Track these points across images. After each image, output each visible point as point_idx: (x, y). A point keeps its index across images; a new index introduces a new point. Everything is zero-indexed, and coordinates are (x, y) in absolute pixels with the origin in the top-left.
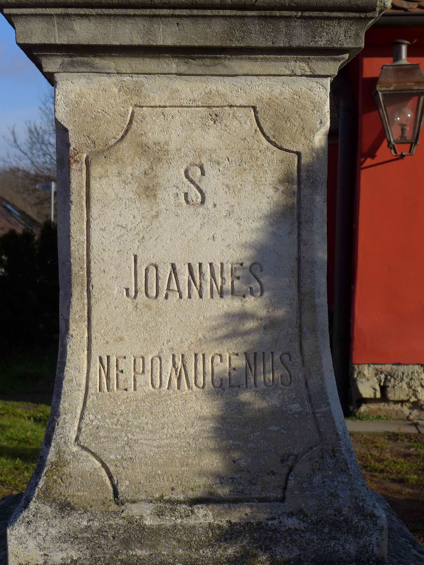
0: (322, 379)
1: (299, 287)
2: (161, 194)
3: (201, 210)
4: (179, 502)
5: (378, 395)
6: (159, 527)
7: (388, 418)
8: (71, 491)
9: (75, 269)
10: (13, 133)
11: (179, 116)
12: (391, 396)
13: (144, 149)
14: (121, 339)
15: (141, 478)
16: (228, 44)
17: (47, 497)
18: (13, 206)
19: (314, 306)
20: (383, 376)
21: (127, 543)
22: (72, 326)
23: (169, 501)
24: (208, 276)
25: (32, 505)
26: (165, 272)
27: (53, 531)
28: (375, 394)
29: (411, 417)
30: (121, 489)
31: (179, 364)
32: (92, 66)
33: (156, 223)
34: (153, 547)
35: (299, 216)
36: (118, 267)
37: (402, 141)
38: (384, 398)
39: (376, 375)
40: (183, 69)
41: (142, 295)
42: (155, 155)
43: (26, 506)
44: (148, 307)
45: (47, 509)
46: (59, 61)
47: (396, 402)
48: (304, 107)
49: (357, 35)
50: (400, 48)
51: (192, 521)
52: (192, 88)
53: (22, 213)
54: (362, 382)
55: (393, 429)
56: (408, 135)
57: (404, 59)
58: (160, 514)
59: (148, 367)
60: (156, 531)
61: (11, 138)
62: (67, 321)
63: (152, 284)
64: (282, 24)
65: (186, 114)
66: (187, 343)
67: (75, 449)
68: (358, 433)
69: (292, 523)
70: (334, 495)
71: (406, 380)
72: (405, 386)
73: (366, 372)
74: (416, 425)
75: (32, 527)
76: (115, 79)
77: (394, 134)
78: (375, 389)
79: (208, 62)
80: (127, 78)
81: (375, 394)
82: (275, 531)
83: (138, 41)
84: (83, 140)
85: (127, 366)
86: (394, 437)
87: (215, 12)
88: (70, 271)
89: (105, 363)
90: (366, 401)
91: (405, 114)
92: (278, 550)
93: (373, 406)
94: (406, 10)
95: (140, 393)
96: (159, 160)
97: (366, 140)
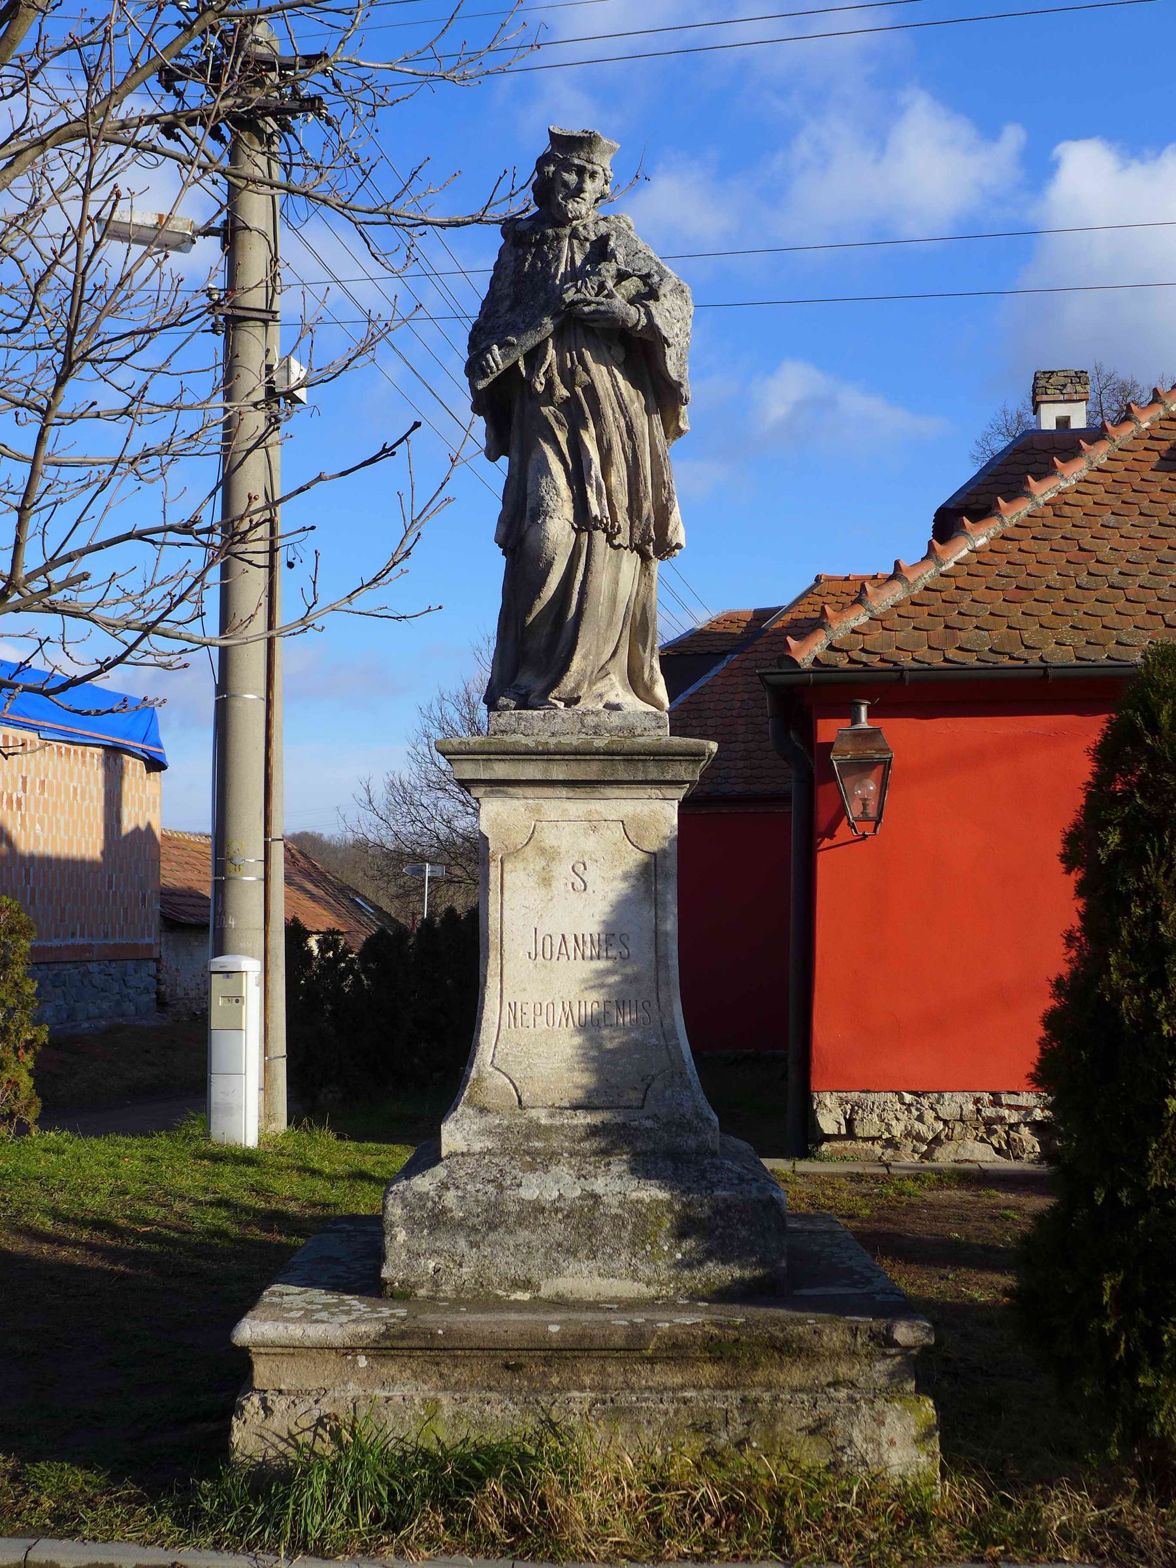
0: (673, 1020)
1: (656, 952)
2: (554, 884)
3: (584, 895)
4: (567, 1108)
5: (844, 1131)
6: (551, 1126)
7: (855, 1158)
8: (487, 1099)
9: (492, 938)
10: (368, 791)
11: (568, 828)
12: (859, 1131)
13: (542, 851)
14: (525, 990)
15: (538, 1091)
16: (602, 778)
17: (470, 1102)
18: (364, 898)
19: (667, 967)
20: (849, 1107)
21: (527, 1137)
22: (489, 980)
23: (559, 1108)
24: (589, 944)
25: (459, 1109)
26: (557, 940)
27: (475, 1127)
28: (839, 1129)
29: (884, 1158)
30: (524, 1098)
31: (567, 1009)
32: (506, 793)
33: (551, 905)
34: (546, 1140)
35: (656, 899)
36: (522, 937)
37: (864, 818)
38: (851, 1135)
39: (841, 1105)
40: (571, 795)
41: (540, 957)
42: (549, 855)
43: (455, 1110)
44: (545, 966)
45: (470, 1111)
46: (483, 789)
47: (866, 1139)
48: (658, 821)
49: (694, 771)
50: (859, 709)
51: (575, 1122)
52: (578, 807)
53: (378, 909)
54: (823, 1114)
55: (857, 1169)
56: (872, 812)
57: (864, 723)
58: (552, 1116)
59: (544, 1011)
60: (549, 1129)
61: (365, 797)
62: (485, 977)
63: (545, 950)
64: (640, 765)
65: (573, 826)
66: (573, 994)
67: (491, 1069)
68: (814, 1174)
69: (648, 1123)
70: (681, 1105)
71: (877, 1111)
72: (876, 1119)
73: (828, 1102)
74: (887, 1166)
75: (459, 1123)
76: (523, 802)
77: (854, 810)
78: (838, 1123)
79: (588, 790)
80: (530, 801)
81: (839, 1129)
82: (636, 1129)
83: (539, 777)
84: (499, 845)
85: (529, 1009)
86: (857, 1178)
87: (593, 757)
88: (488, 939)
89: (513, 1007)
90: (829, 1138)
91: (866, 786)
92: (638, 1144)
93: (837, 1145)
94: (865, 664)
95: (538, 1030)
96: (554, 859)
97: (823, 817)
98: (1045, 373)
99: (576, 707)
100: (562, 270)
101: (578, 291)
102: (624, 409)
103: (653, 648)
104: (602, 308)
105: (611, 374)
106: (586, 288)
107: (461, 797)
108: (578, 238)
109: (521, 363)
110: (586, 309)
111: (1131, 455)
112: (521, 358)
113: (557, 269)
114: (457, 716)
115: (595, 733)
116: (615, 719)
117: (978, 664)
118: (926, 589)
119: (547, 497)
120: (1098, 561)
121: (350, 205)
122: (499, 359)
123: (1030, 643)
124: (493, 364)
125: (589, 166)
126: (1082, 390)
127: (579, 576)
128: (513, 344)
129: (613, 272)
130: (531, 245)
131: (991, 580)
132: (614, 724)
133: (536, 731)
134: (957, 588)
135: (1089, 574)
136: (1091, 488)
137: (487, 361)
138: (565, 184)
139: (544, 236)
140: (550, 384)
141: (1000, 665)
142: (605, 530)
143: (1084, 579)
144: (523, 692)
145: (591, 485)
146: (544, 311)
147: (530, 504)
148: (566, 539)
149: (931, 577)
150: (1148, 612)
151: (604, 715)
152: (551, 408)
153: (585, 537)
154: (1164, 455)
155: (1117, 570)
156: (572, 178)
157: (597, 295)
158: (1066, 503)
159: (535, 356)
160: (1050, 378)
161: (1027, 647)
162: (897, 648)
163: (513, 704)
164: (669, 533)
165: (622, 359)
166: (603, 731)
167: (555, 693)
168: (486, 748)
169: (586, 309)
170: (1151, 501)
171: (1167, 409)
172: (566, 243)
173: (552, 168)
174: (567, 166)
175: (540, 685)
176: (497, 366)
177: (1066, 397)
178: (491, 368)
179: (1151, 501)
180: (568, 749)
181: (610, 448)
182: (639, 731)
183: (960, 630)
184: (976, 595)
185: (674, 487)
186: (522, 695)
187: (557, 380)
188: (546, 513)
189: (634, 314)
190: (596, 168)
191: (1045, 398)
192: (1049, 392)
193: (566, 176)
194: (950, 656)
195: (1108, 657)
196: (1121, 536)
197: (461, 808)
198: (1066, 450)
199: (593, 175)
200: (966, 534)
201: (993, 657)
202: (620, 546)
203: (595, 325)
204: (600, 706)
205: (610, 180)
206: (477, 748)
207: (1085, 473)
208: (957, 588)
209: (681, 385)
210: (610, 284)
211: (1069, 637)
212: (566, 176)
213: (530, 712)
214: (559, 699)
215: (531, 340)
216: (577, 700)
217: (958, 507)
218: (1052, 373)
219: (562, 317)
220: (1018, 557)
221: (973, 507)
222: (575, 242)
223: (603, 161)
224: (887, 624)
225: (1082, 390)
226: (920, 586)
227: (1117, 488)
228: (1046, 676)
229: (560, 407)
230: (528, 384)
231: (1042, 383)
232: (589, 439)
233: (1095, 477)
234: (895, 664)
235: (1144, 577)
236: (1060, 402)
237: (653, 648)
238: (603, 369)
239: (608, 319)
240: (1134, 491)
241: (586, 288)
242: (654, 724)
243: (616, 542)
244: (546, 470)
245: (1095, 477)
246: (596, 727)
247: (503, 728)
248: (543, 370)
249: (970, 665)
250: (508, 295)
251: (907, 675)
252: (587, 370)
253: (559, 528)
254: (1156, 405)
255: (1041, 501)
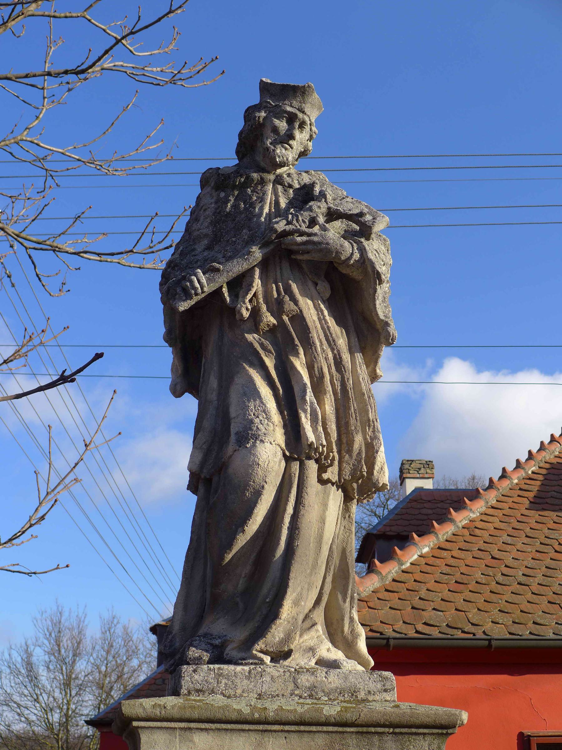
64: (376, 738)
98: (408, 461)
99: (286, 663)
100: (266, 210)
101: (289, 223)
102: (331, 342)
103: (352, 598)
104: (315, 239)
105: (317, 308)
106: (298, 221)
107: (18, 711)
108: (282, 184)
109: (225, 290)
110: (299, 239)
111: (511, 499)
112: (225, 285)
113: (262, 209)
114: (19, 659)
115: (311, 696)
116: (333, 680)
117: (440, 636)
118: (394, 580)
119: (257, 421)
120: (506, 566)
121: (23, 235)
122: (204, 280)
123: (474, 621)
124: (197, 285)
125: (300, 115)
126: (430, 472)
127: (290, 510)
128: (218, 270)
129: (324, 209)
130: (234, 187)
131: (438, 576)
132: (333, 686)
133: (239, 691)
134: (415, 581)
135: (502, 574)
136: (490, 519)
137: (191, 282)
138: (275, 130)
139: (249, 180)
140: (255, 313)
141: (455, 637)
142: (317, 461)
143: (500, 578)
144: (217, 642)
145: (305, 411)
146: (251, 241)
147: (234, 428)
148: (276, 467)
149: (396, 572)
150: (549, 602)
151: (321, 672)
152: (256, 336)
153: (296, 466)
154: (532, 500)
155: (521, 573)
156: (282, 125)
157: (309, 227)
158: (476, 528)
159: (239, 284)
160: (411, 464)
161: (473, 624)
162: (381, 622)
163: (206, 656)
164: (375, 472)
165: (328, 294)
166: (320, 694)
167: (261, 645)
168: (188, 714)
169: (299, 239)
170: (531, 528)
171: (526, 473)
172: (270, 187)
173: (263, 114)
174: (279, 113)
175: (239, 635)
176: (202, 288)
177: (421, 475)
178: (195, 289)
179: (531, 528)
180: (291, 717)
181: (322, 376)
182: (362, 695)
183: (423, 610)
184: (429, 586)
185: (378, 425)
186: (215, 647)
187: (264, 307)
188: (256, 437)
189: (348, 248)
190: (307, 119)
191: (408, 475)
192: (411, 472)
193: (277, 122)
194: (396, 628)
195: (530, 633)
196: (518, 550)
197: (17, 717)
198: (442, 501)
199: (302, 125)
200: (415, 544)
201: (450, 631)
202: (328, 481)
203: (306, 257)
204: (313, 663)
205: (314, 136)
206: (176, 713)
207: (484, 509)
208: (415, 581)
209: (387, 324)
210: (321, 220)
211: (500, 618)
212: (277, 122)
213: (232, 667)
214: (265, 653)
215: (237, 267)
216: (287, 654)
217: (378, 533)
218: (413, 461)
219: (272, 247)
220: (452, 562)
221: (388, 533)
222: (280, 188)
223: (312, 113)
224: (370, 604)
225: (430, 472)
226: (390, 578)
227: (506, 519)
228: (490, 645)
229: (265, 335)
230: (233, 311)
231: (406, 466)
232: (299, 363)
233: (491, 511)
234: (381, 634)
235: (540, 578)
236: (418, 478)
237: (352, 598)
238: (310, 302)
239: (321, 250)
240: (518, 521)
241: (298, 221)
242: (379, 686)
243: (325, 476)
244: (256, 394)
245: (491, 511)
246: (312, 688)
247: (198, 687)
248: (249, 296)
249: (435, 636)
250: (206, 235)
251: (392, 642)
252: (296, 302)
253: (269, 452)
254: (519, 469)
255: (460, 525)
